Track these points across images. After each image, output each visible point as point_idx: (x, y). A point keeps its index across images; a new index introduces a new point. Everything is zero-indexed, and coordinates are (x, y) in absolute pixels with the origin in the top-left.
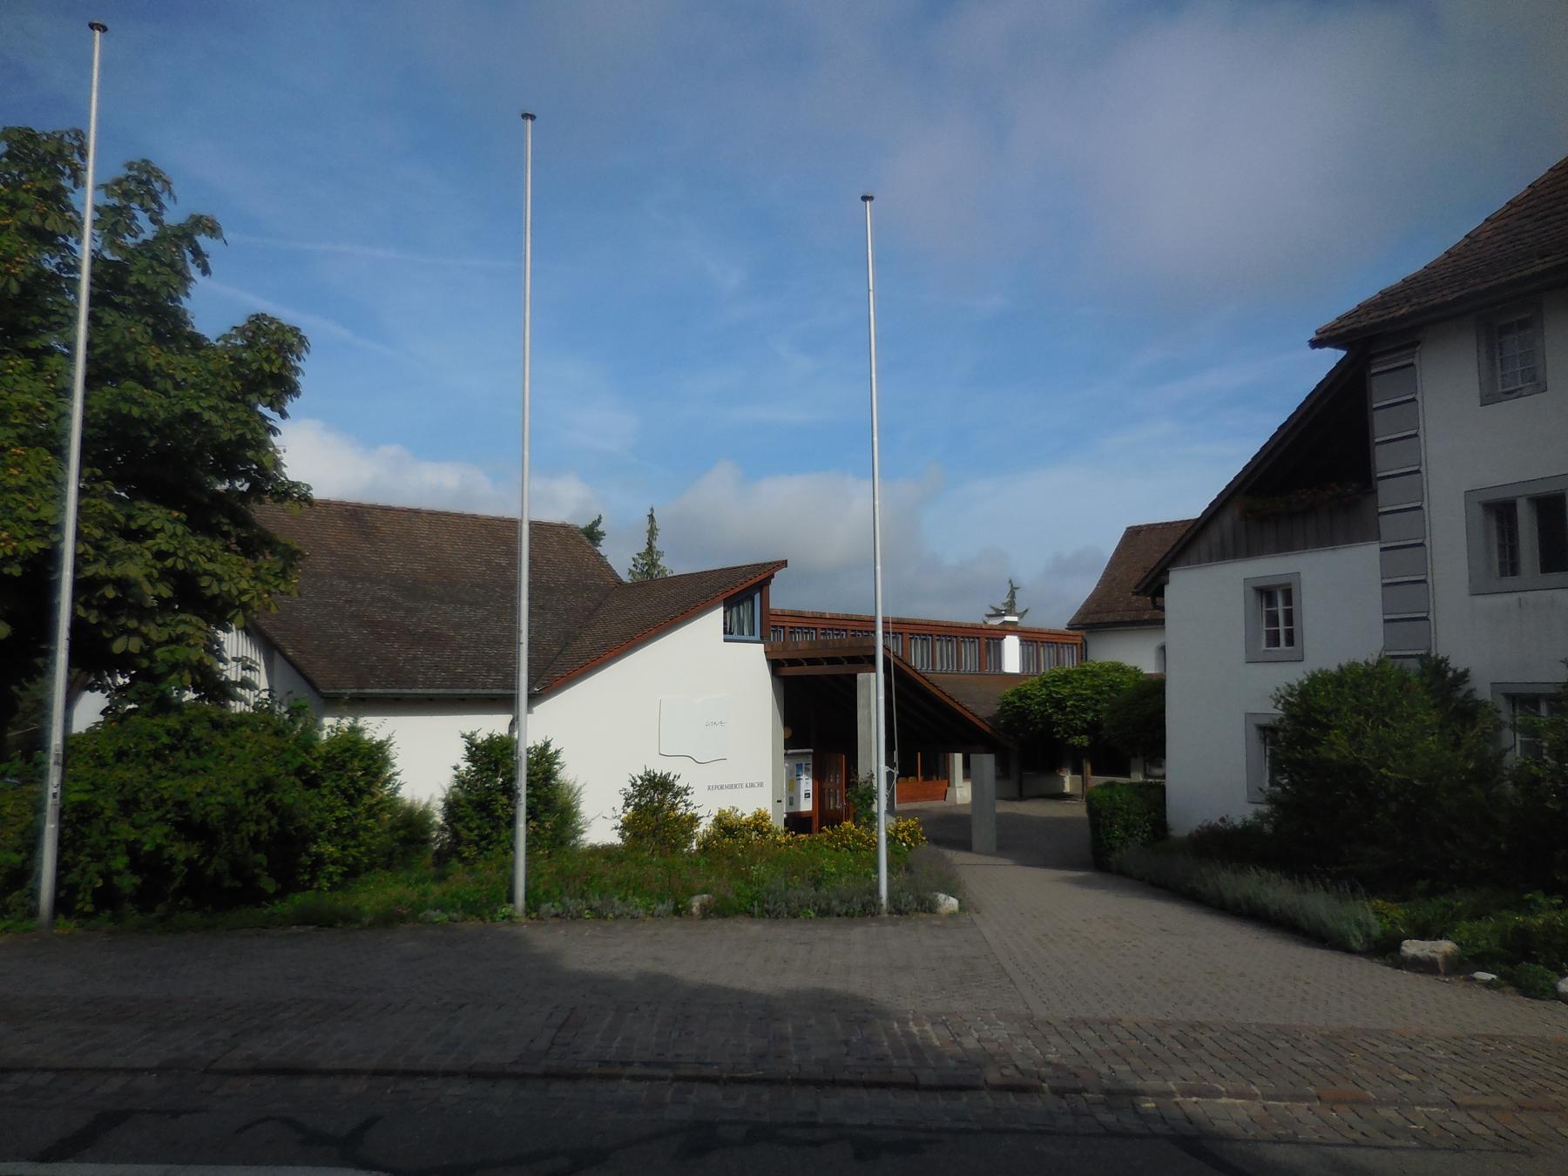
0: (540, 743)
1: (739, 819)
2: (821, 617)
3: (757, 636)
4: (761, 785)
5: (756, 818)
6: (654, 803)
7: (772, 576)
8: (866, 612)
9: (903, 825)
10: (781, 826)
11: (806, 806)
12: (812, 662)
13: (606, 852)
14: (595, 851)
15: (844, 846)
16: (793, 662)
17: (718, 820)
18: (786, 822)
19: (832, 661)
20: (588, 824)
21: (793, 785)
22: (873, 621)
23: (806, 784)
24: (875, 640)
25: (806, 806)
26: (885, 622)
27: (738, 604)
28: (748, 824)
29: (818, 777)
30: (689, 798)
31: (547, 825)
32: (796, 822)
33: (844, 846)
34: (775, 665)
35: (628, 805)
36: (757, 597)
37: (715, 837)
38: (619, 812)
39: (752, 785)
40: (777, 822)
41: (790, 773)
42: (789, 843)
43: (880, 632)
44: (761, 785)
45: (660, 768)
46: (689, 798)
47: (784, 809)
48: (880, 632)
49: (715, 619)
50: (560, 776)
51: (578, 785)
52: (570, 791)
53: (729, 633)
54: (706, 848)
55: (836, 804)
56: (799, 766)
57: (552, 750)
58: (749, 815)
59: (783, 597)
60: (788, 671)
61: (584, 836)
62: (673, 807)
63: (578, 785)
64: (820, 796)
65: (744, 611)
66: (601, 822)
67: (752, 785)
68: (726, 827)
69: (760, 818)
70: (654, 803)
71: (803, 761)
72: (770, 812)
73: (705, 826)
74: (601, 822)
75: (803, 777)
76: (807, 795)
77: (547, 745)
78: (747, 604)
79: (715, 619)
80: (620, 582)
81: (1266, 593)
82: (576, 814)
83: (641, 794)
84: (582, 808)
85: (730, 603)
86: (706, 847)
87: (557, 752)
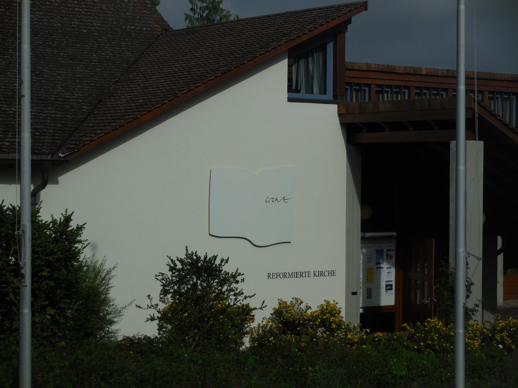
0: (59, 217)
1: (302, 313)
2: (415, 73)
3: (330, 95)
4: (332, 273)
5: (323, 311)
6: (198, 288)
7: (349, 21)
8: (442, 65)
9: (502, 324)
10: (356, 322)
11: (388, 299)
12: (396, 126)
13: (137, 346)
14: (131, 343)
15: (427, 346)
16: (373, 127)
17: (278, 313)
18: (363, 317)
19: (420, 126)
20: (118, 313)
21: (371, 275)
22: (454, 76)
23: (388, 274)
24: (455, 98)
25: (388, 299)
26: (469, 78)
27: (306, 55)
28: (313, 318)
29: (402, 267)
30: (240, 286)
31: (68, 313)
32: (374, 317)
33: (427, 346)
34: (351, 130)
35: (165, 292)
36: (330, 47)
37: (271, 332)
38: (156, 300)
39: (321, 274)
40: (349, 313)
41: (368, 259)
42: (362, 341)
43: (462, 87)
44: (332, 273)
45: (205, 249)
46: (240, 286)
47: (360, 301)
48: (462, 87)
49: (276, 75)
50: (85, 256)
51: (107, 266)
52: (98, 273)
53: (296, 91)
54: (261, 345)
55: (423, 298)
56: (379, 253)
57: (73, 225)
58: (315, 308)
59: (361, 48)
60: (366, 138)
61: (114, 327)
62: (220, 296)
63: (107, 266)
64: (403, 287)
65: (314, 64)
66: (135, 311)
67: (321, 274)
68: (288, 320)
69: (329, 311)
70: (198, 288)
71: (384, 247)
72: (342, 305)
73: (261, 318)
74: (135, 311)
75: (385, 265)
76: (389, 287)
77: (68, 219)
78: (318, 56)
79: (276, 75)
80: (167, 29)
81: (391, 285)
82: (106, 301)
83: (181, 280)
84: (112, 294)
85: (297, 55)
86: (261, 340)
87: (80, 228)
